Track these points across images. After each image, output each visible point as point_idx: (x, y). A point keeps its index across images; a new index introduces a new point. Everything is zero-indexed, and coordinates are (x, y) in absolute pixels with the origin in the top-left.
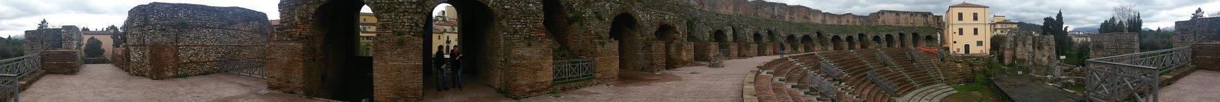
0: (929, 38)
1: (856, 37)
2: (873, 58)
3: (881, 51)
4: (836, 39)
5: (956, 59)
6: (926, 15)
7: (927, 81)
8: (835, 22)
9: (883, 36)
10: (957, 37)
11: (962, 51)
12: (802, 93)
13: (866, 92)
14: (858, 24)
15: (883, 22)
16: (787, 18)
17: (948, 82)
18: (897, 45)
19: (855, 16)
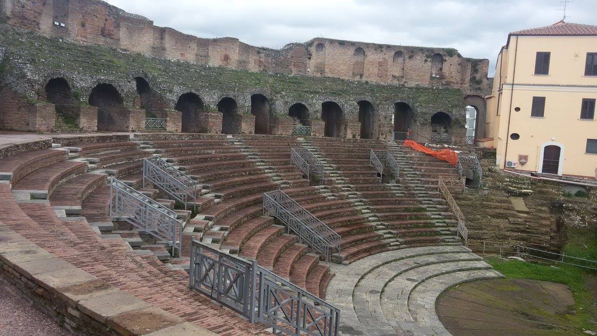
0: (441, 120)
1: (244, 102)
2: (284, 161)
3: (308, 144)
4: (190, 103)
5: (513, 184)
6: (438, 56)
7: (419, 233)
8: (191, 56)
9: (315, 105)
10: (523, 122)
11: (536, 164)
12: (95, 229)
13: (258, 242)
14: (253, 68)
15: (320, 68)
16: (46, 27)
17: (477, 243)
18: (351, 132)
19: (246, 48)
